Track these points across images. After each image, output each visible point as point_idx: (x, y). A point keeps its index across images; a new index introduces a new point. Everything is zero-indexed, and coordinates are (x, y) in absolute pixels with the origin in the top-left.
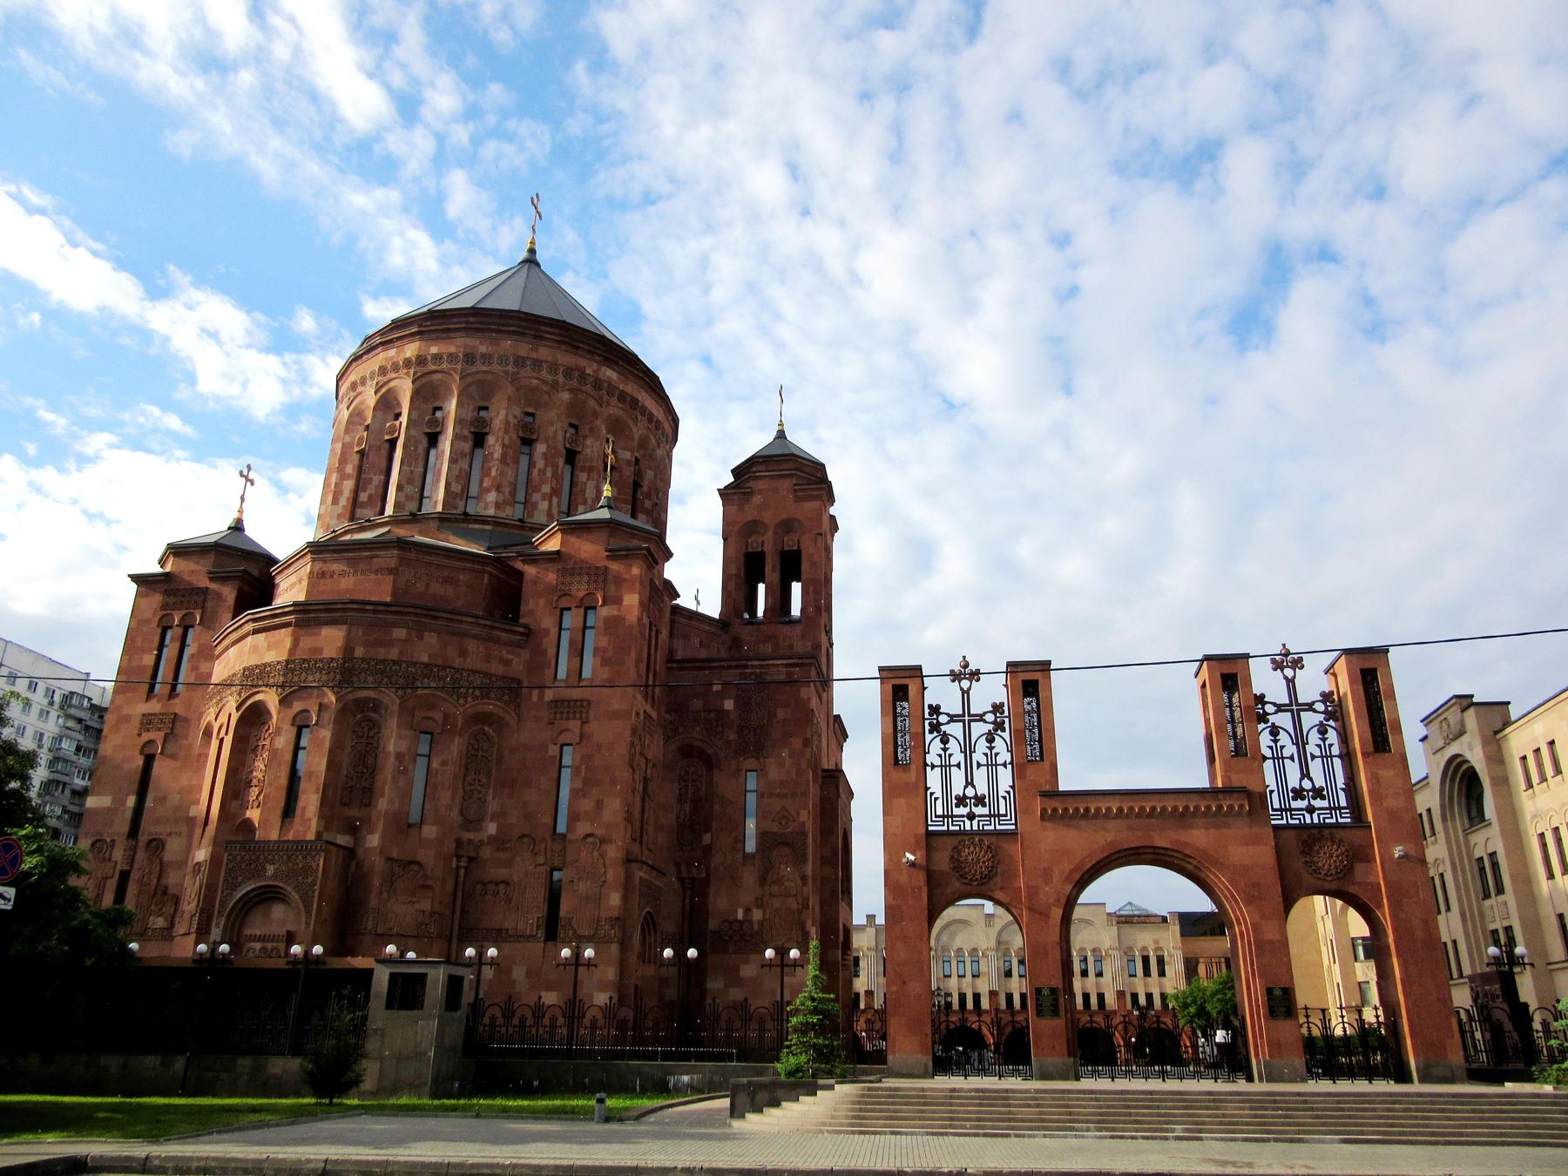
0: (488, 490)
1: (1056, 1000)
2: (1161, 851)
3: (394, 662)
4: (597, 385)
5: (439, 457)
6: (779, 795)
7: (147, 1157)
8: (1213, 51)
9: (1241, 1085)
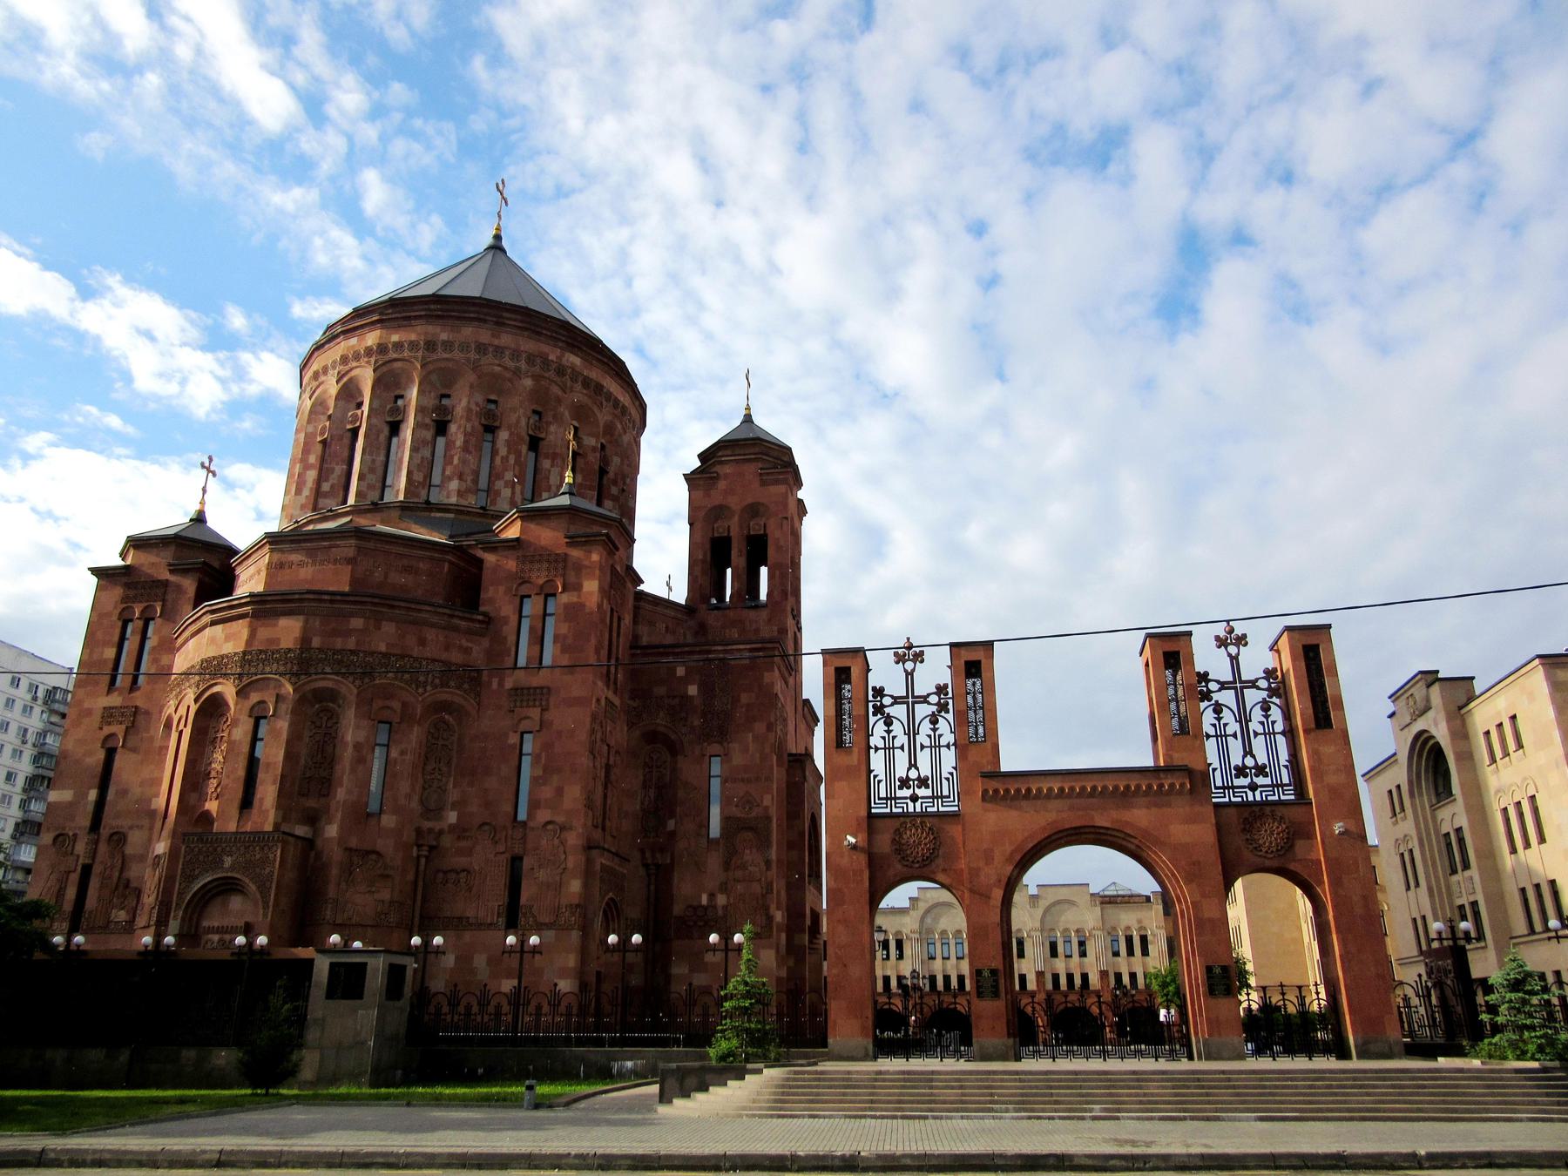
0: (450, 479)
1: (996, 981)
2: (1102, 831)
3: (352, 652)
4: (561, 371)
5: (401, 445)
6: (743, 780)
7: (43, 1150)
8: (1110, 37)
9: (1184, 1065)
